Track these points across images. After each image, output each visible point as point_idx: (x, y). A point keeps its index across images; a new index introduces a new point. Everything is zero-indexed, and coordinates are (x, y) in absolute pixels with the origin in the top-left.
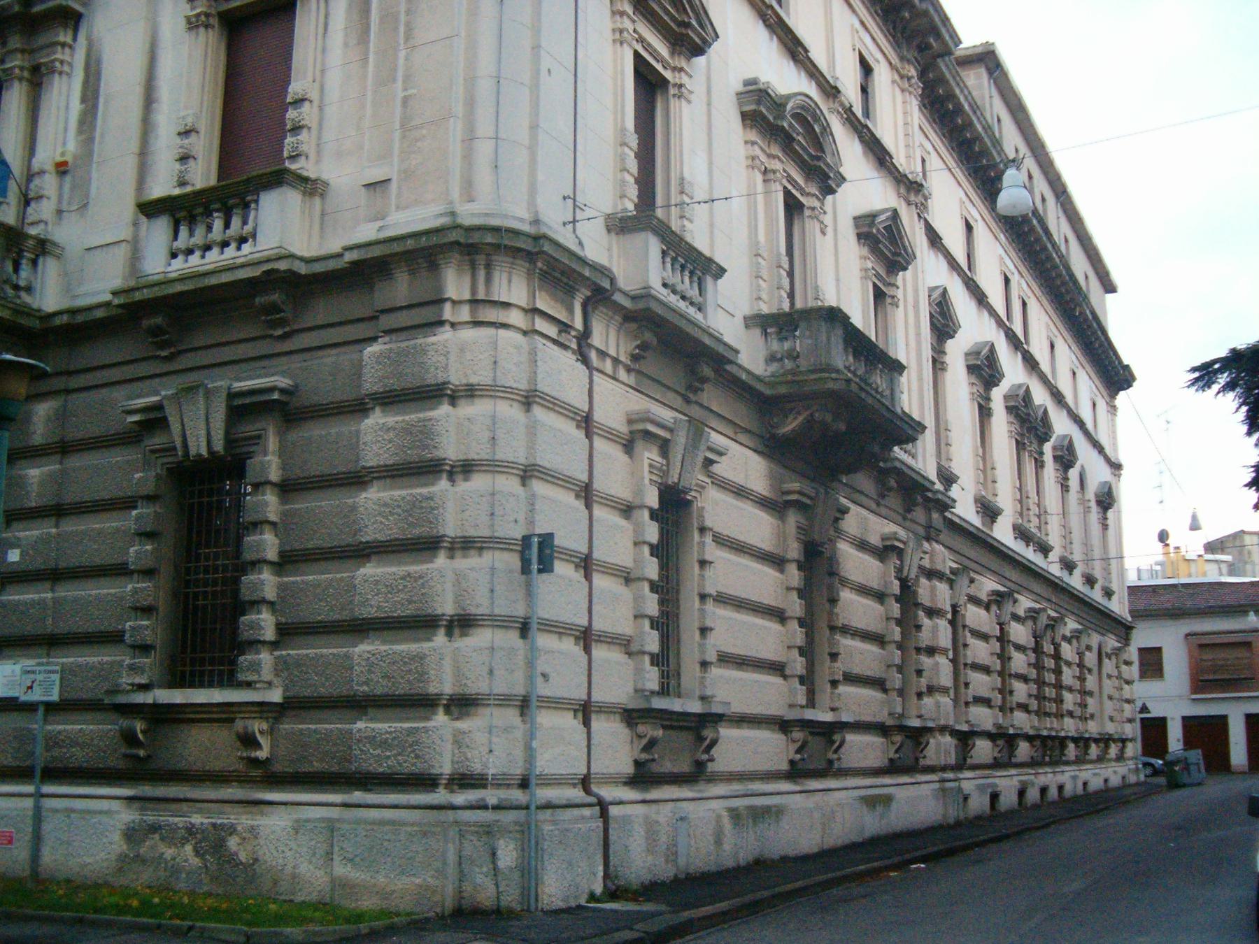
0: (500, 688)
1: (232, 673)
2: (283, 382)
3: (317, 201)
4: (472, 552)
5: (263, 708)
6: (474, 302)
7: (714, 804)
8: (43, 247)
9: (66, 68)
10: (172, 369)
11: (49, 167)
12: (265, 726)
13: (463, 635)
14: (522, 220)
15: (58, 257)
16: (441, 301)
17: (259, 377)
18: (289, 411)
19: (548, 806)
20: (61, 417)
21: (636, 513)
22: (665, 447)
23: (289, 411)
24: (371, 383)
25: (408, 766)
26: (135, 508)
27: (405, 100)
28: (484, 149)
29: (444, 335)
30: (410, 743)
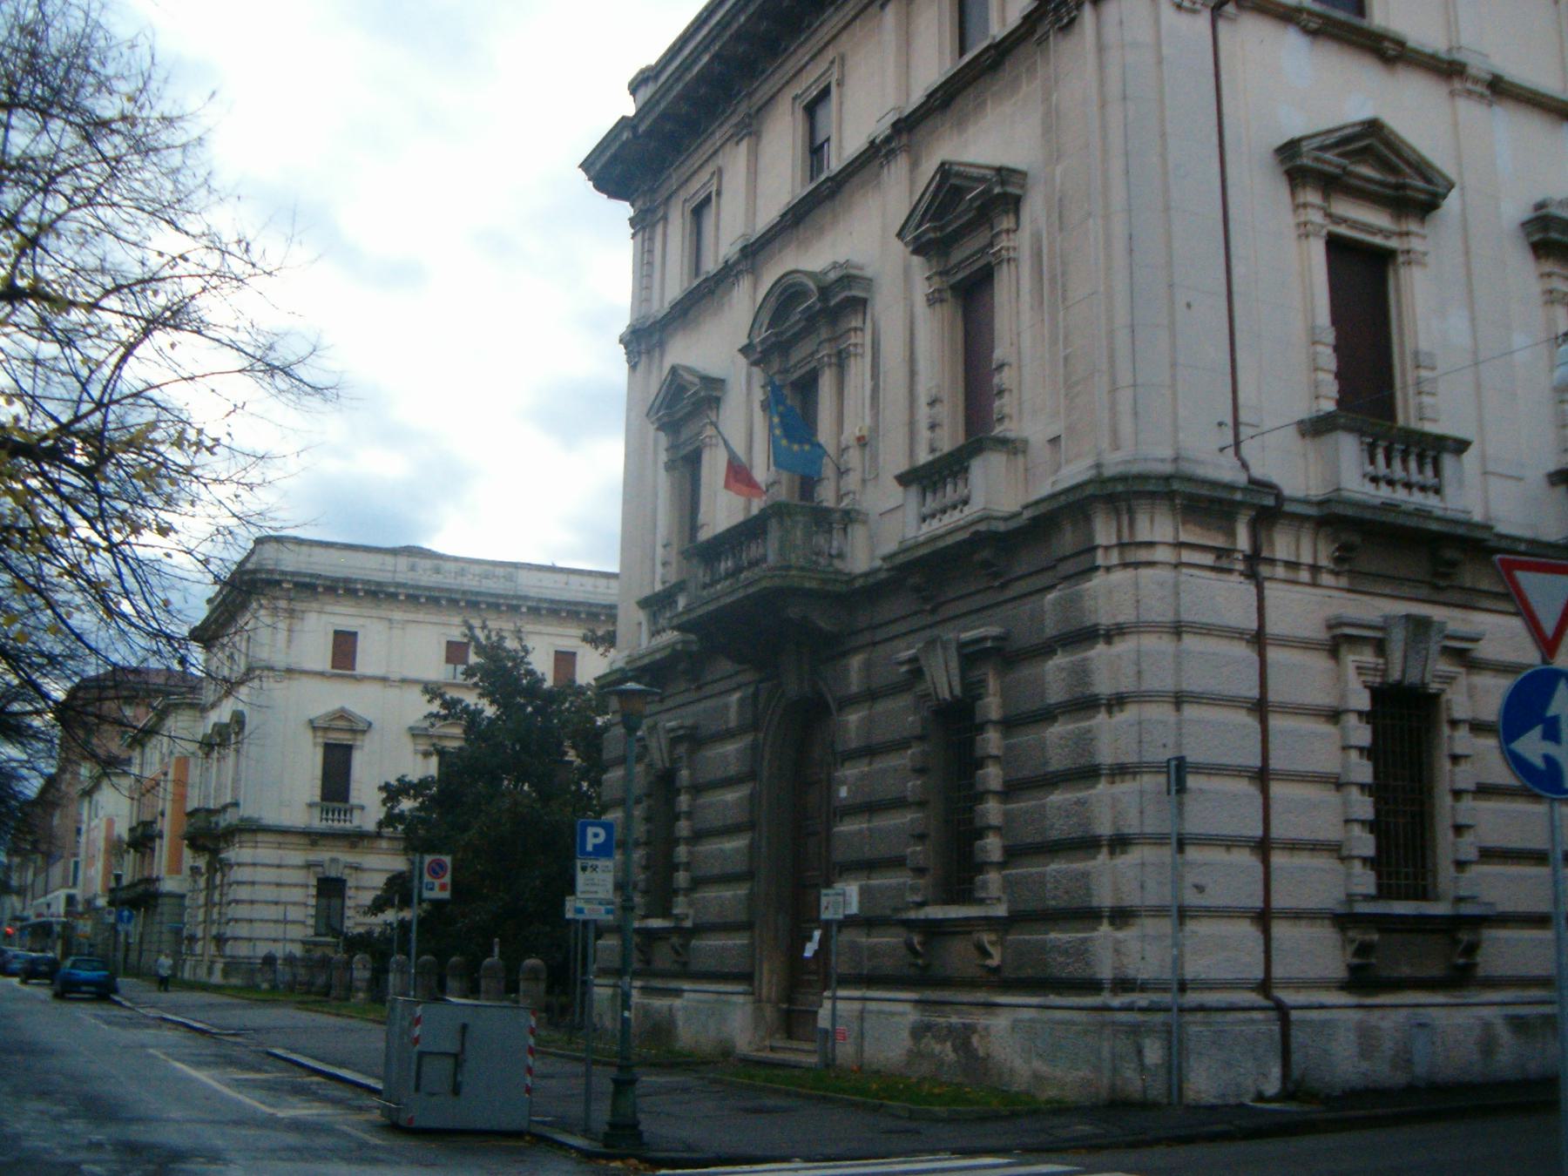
0: (1152, 899)
1: (971, 891)
2: (994, 630)
3: (1020, 458)
4: (1128, 777)
5: (990, 923)
6: (1121, 546)
7: (1486, 1012)
8: (849, 517)
9: (1012, 254)
10: (1001, 598)
11: (852, 442)
12: (993, 937)
13: (1124, 852)
14: (1163, 460)
15: (865, 522)
16: (1093, 549)
17: (972, 629)
18: (1007, 655)
19: (1201, 1008)
20: (868, 666)
21: (1344, 718)
22: (1380, 647)
23: (1007, 655)
24: (1051, 629)
25: (1074, 970)
26: (909, 747)
27: (1066, 359)
28: (1125, 399)
29: (1098, 581)
30: (1081, 952)
